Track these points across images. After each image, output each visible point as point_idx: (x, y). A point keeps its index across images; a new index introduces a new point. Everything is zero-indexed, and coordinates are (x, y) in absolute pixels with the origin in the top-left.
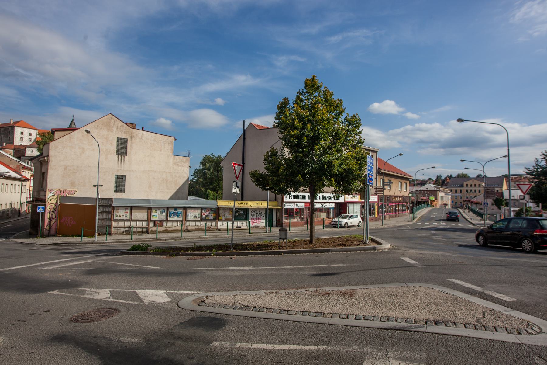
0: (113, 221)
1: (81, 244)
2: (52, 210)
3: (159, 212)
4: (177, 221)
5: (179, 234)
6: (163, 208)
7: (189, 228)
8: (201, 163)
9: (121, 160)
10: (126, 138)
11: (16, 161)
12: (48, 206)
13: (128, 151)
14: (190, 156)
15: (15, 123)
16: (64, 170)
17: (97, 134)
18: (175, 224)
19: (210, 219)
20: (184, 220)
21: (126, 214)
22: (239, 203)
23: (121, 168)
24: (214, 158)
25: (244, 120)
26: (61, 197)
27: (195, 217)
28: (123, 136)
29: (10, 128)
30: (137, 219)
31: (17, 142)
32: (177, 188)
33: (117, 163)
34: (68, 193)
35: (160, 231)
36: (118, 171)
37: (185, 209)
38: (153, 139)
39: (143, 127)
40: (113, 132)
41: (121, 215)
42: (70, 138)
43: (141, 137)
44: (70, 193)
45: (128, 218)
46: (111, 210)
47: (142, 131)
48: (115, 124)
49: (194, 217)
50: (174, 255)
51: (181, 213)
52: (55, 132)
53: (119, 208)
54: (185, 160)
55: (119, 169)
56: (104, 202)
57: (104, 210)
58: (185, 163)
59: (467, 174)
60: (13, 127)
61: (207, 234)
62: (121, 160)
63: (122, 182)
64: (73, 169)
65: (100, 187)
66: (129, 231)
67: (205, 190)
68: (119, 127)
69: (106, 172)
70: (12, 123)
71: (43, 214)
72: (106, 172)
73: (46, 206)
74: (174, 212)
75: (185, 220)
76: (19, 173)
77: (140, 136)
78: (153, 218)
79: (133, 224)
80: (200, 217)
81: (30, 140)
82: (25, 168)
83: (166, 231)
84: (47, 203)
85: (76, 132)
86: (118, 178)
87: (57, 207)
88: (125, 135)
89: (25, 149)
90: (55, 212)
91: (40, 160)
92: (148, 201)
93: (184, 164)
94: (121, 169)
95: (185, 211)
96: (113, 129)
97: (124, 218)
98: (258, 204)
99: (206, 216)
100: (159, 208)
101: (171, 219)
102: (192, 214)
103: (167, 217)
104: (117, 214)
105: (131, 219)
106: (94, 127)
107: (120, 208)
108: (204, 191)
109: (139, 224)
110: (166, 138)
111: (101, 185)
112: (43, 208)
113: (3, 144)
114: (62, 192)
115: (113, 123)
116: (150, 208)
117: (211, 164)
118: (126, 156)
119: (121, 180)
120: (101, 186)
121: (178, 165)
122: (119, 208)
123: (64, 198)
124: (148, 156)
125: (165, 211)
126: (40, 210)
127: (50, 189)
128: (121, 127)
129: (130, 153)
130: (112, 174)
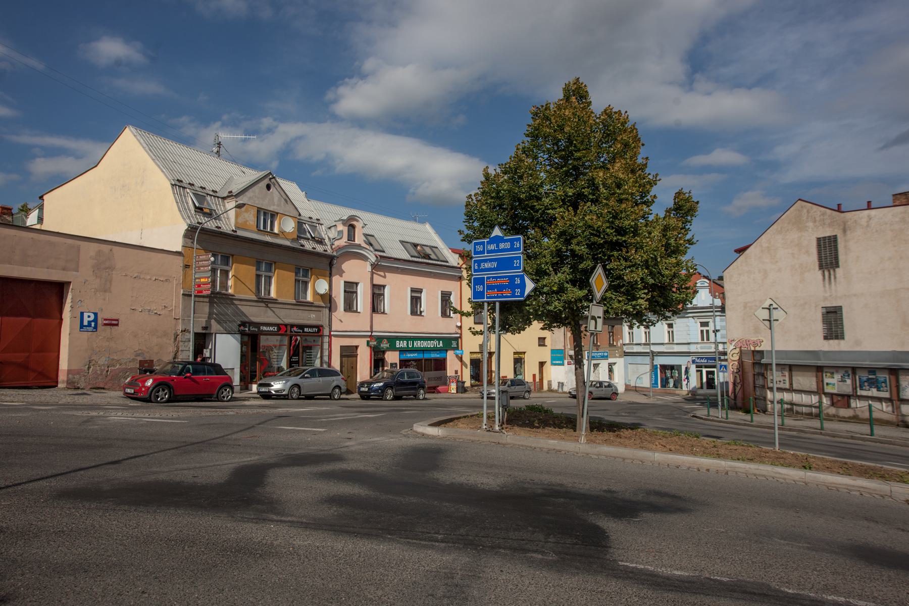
0: (823, 396)
2: (735, 371)
3: (837, 377)
4: (880, 400)
9: (830, 277)
10: (834, 234)
13: (842, 257)
20: (895, 397)
21: (784, 378)
30: (801, 389)
33: (822, 285)
35: (844, 418)
36: (825, 299)
39: (869, 203)
48: (810, 214)
51: (885, 382)
55: (827, 295)
62: (830, 277)
63: (836, 321)
68: (818, 219)
74: (869, 379)
77: (864, 222)
78: (828, 389)
79: (796, 398)
88: (831, 229)
90: (739, 373)
94: (830, 296)
95: (893, 378)
100: (837, 368)
101: (864, 393)
103: (855, 389)
109: (805, 399)
114: (744, 343)
115: (806, 214)
116: (819, 370)
118: (837, 270)
125: (849, 376)
127: (731, 339)
128: (822, 217)
130: (816, 307)
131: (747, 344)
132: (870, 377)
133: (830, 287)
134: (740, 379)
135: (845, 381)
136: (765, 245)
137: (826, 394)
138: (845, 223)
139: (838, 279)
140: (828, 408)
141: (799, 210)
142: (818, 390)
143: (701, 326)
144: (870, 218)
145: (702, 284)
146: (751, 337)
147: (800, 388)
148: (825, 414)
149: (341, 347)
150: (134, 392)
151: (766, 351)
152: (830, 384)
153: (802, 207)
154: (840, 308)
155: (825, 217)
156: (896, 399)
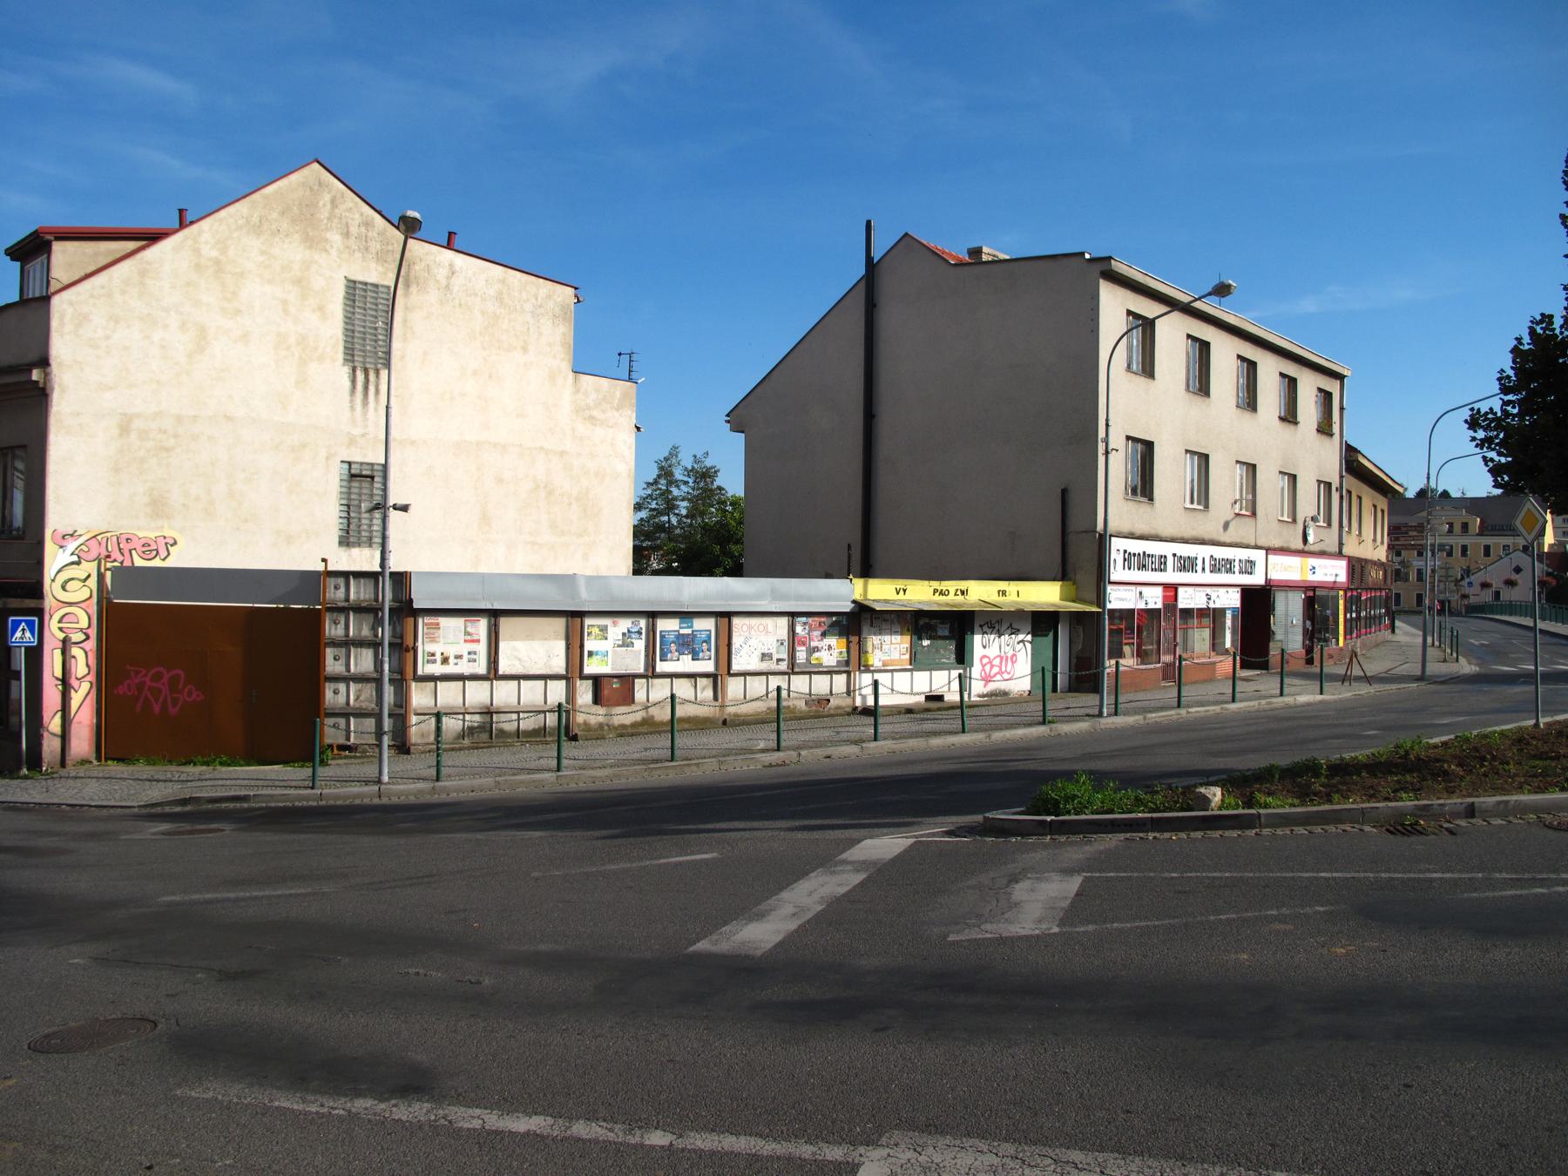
4: (692, 676)
9: (366, 388)
12: (56, 617)
14: (634, 375)
16: (121, 435)
17: (261, 259)
18: (683, 689)
19: (825, 663)
20: (724, 670)
21: (472, 647)
22: (935, 591)
23: (366, 426)
25: (868, 224)
27: (765, 657)
34: (140, 549)
36: (352, 441)
37: (725, 617)
38: (492, 292)
40: (326, 251)
41: (451, 652)
42: (143, 273)
43: (444, 282)
44: (149, 549)
49: (763, 655)
51: (708, 641)
52: (54, 243)
54: (618, 394)
55: (357, 431)
58: (618, 410)
59: (634, 526)
62: (366, 388)
64: (160, 430)
68: (354, 230)
69: (304, 446)
72: (304, 446)
73: (47, 617)
77: (442, 273)
78: (592, 667)
79: (504, 694)
80: (785, 656)
84: (49, 603)
88: (380, 269)
92: (566, 581)
93: (616, 414)
96: (328, 235)
97: (464, 668)
98: (1004, 593)
102: (753, 642)
104: (430, 647)
105: (496, 670)
106: (248, 222)
111: (401, 502)
112: (30, 625)
115: (329, 206)
116: (575, 617)
120: (405, 508)
121: (592, 418)
123: (128, 576)
124: (475, 373)
126: (18, 634)
128: (363, 229)
129: (403, 357)
130: (327, 458)
133: (365, 413)
134: (87, 665)
136: (210, 252)
141: (311, 189)
142: (567, 672)
146: (139, 529)
149: (1153, 442)
152: (597, 653)
153: (320, 184)
156: (578, 675)
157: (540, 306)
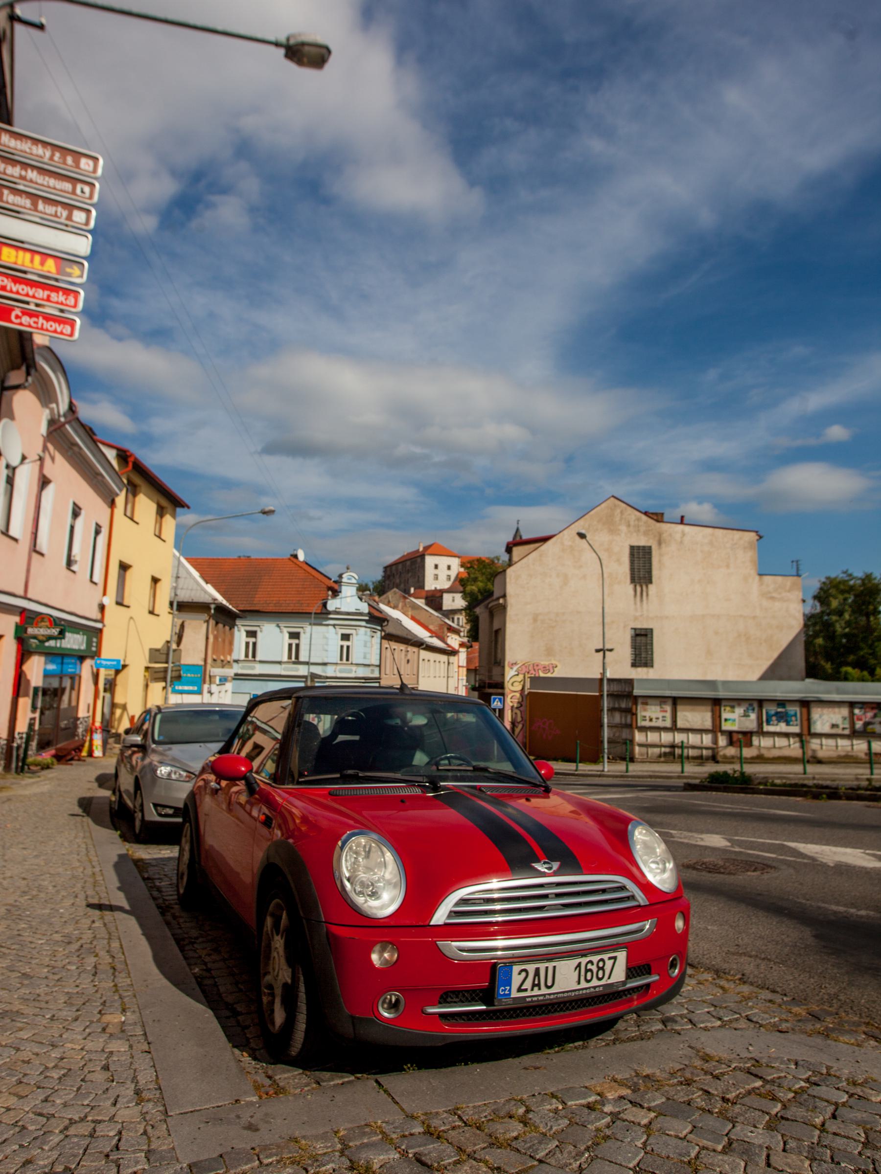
0: (719, 734)
1: (577, 775)
2: (516, 705)
3: (739, 711)
4: (787, 735)
5: (798, 768)
6: (751, 702)
7: (821, 754)
8: (815, 597)
11: (437, 617)
12: (510, 696)
13: (655, 573)
14: (800, 572)
15: (426, 548)
18: (781, 742)
20: (805, 732)
21: (664, 714)
24: (852, 583)
26: (530, 677)
27: (834, 726)
28: (642, 542)
29: (419, 560)
31: (430, 585)
32: (775, 655)
36: (636, 619)
37: (806, 704)
41: (654, 716)
44: (546, 669)
45: (668, 723)
46: (630, 704)
47: (681, 527)
50: (824, 796)
51: (795, 715)
53: (647, 699)
55: (638, 614)
56: (615, 688)
57: (617, 706)
58: (789, 591)
60: (422, 556)
61: (875, 771)
63: (646, 645)
65: (607, 653)
66: (672, 754)
67: (832, 669)
68: (632, 523)
70: (421, 549)
71: (502, 712)
74: (777, 714)
75: (806, 734)
76: (443, 640)
77: (678, 536)
78: (726, 727)
79: (679, 737)
80: (847, 726)
81: (449, 577)
82: (451, 629)
83: (760, 759)
84: (507, 691)
85: (550, 543)
86: (637, 635)
87: (524, 699)
89: (442, 597)
90: (522, 709)
91: (490, 605)
92: (712, 684)
94: (641, 616)
95: (805, 710)
96: (620, 527)
97: (660, 724)
99: (866, 724)
100: (739, 701)
103: (760, 724)
104: (644, 714)
105: (676, 725)
107: (649, 701)
108: (830, 671)
109: (694, 739)
110: (737, 535)
112: (500, 699)
113: (409, 590)
114: (531, 668)
115: (619, 515)
116: (716, 703)
117: (845, 599)
118: (650, 586)
119: (643, 638)
120: (611, 650)
122: (647, 699)
123: (536, 681)
125: (753, 710)
126: (495, 703)
128: (636, 522)
131: (534, 670)
132: (779, 710)
135: (749, 716)
137: (723, 732)
138: (660, 534)
139: (650, 597)
140: (725, 747)
143: (247, 636)
144: (683, 534)
145: (349, 579)
147: (687, 725)
148: (721, 756)
150: (632, 971)
151: (638, 680)
152: (729, 720)
154: (651, 630)
155: (640, 524)
157: (736, 544)
